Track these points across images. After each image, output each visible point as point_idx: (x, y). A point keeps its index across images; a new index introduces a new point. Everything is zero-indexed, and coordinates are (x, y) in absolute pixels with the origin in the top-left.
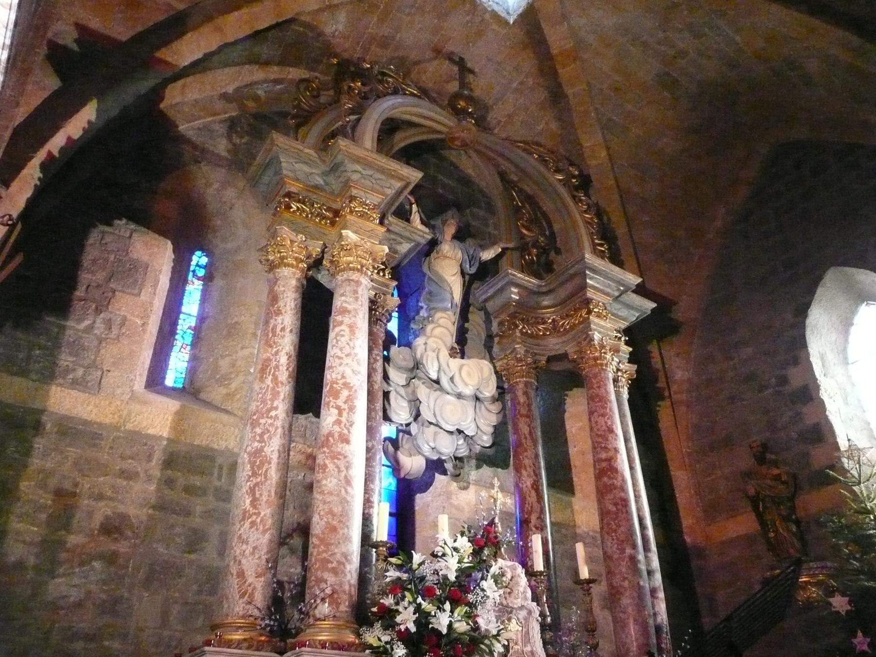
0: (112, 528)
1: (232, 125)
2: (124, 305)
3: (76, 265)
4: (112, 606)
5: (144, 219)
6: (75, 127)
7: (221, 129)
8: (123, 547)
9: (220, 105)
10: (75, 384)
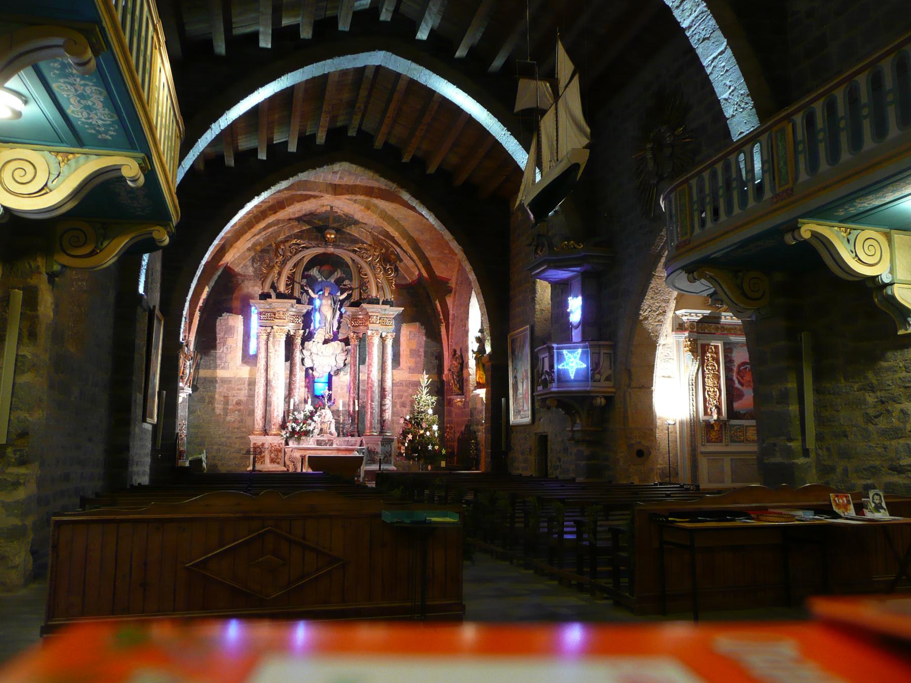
0: (238, 403)
1: (253, 260)
2: (230, 342)
3: (215, 333)
4: (241, 421)
5: (230, 311)
6: (204, 296)
7: (249, 263)
8: (242, 407)
9: (247, 254)
10: (223, 368)
